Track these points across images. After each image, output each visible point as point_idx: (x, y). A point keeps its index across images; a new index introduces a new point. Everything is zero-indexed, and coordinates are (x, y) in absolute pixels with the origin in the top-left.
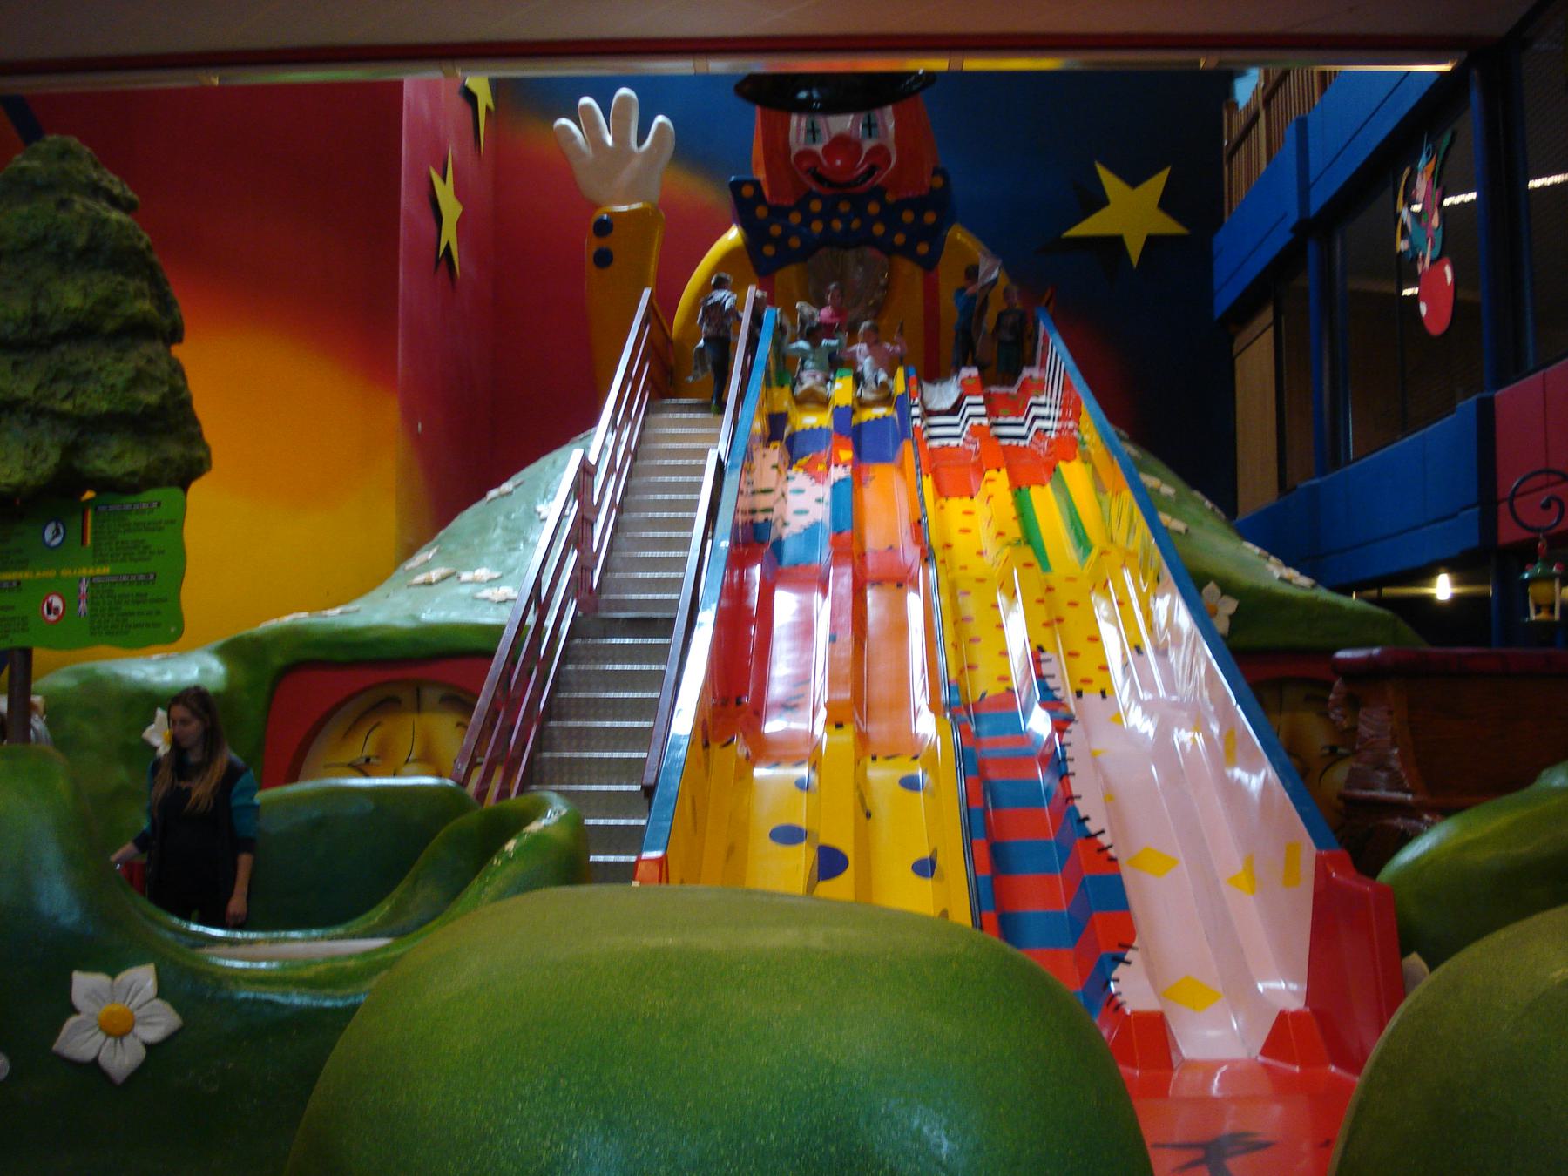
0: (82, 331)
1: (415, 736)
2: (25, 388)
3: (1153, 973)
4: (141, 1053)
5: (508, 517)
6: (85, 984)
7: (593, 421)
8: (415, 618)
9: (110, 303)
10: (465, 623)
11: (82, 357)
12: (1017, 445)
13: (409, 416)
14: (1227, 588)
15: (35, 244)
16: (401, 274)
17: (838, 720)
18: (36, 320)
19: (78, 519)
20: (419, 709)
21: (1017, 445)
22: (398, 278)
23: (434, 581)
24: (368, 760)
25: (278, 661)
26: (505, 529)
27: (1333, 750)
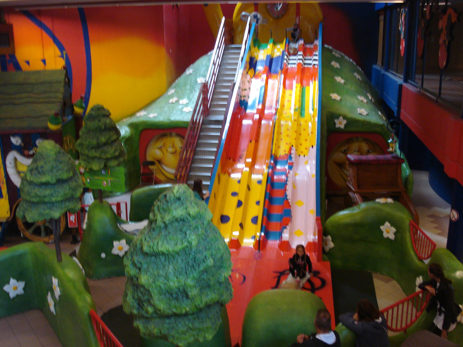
0: (105, 144)
1: (168, 173)
2: (98, 155)
3: (291, 234)
4: (124, 252)
5: (191, 81)
6: (116, 243)
7: (212, 48)
8: (170, 120)
9: (109, 139)
10: (180, 121)
11: (105, 148)
12: (309, 67)
13: (168, 51)
14: (345, 118)
15: (96, 129)
16: (164, 17)
17: (241, 182)
18: (98, 144)
19: (107, 171)
20: (171, 136)
21: (309, 67)
22: (163, 18)
23: (174, 102)
24: (161, 147)
25: (141, 128)
26: (190, 86)
27: (368, 151)
